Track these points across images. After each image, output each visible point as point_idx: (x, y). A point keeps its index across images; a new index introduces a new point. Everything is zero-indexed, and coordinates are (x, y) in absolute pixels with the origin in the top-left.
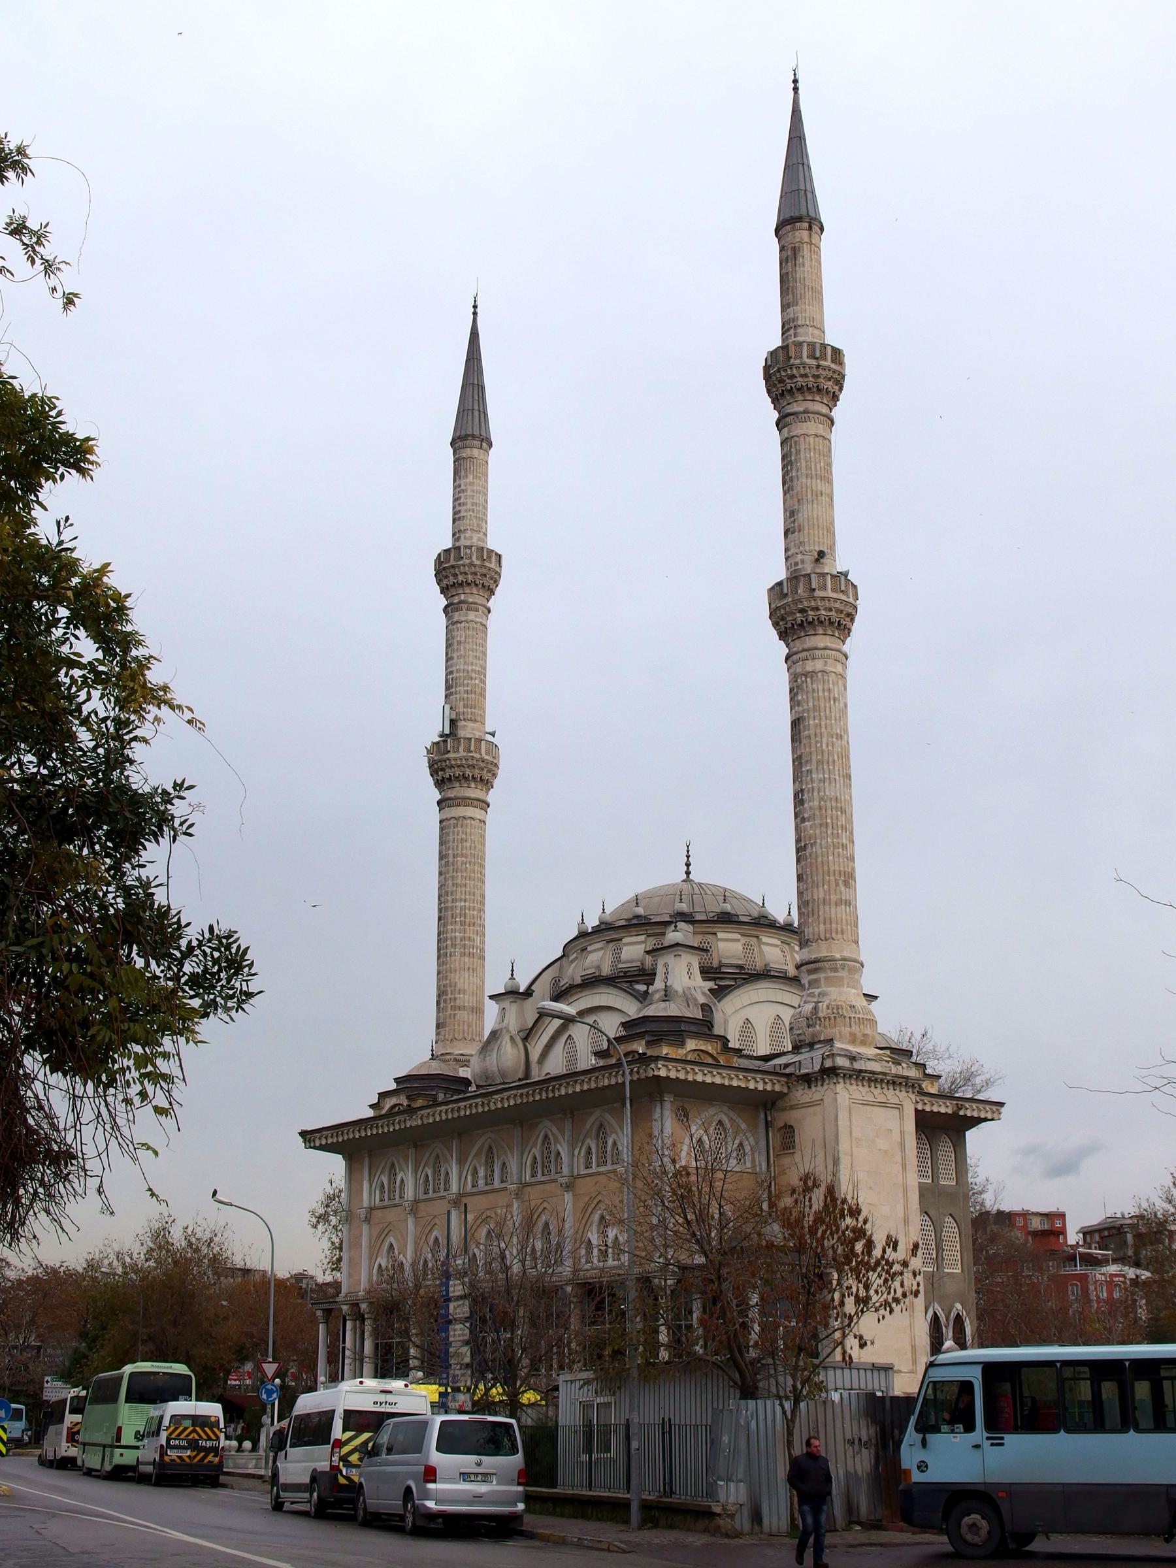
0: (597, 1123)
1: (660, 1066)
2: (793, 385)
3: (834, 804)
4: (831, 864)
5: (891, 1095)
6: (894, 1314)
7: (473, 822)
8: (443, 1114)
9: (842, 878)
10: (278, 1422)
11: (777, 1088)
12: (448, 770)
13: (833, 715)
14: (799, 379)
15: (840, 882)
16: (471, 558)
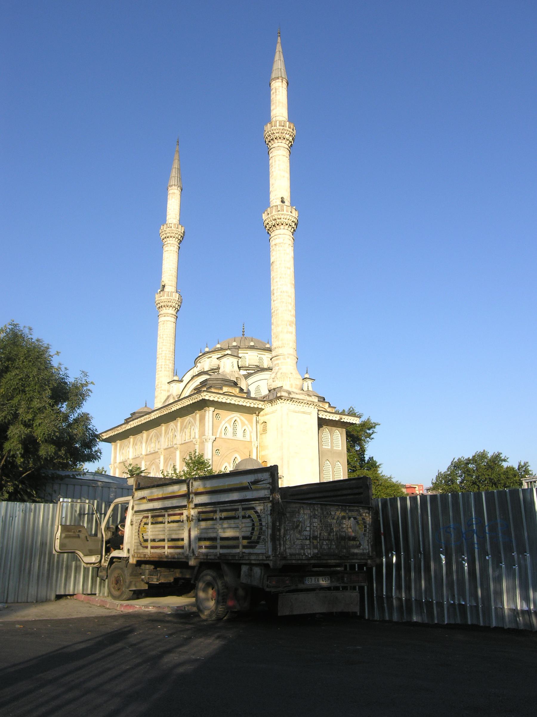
0: (188, 422)
2: (273, 137)
5: (306, 408)
6: (52, 360)
8: (137, 423)
10: (106, 554)
12: (161, 303)
14: (276, 134)
16: (171, 228)
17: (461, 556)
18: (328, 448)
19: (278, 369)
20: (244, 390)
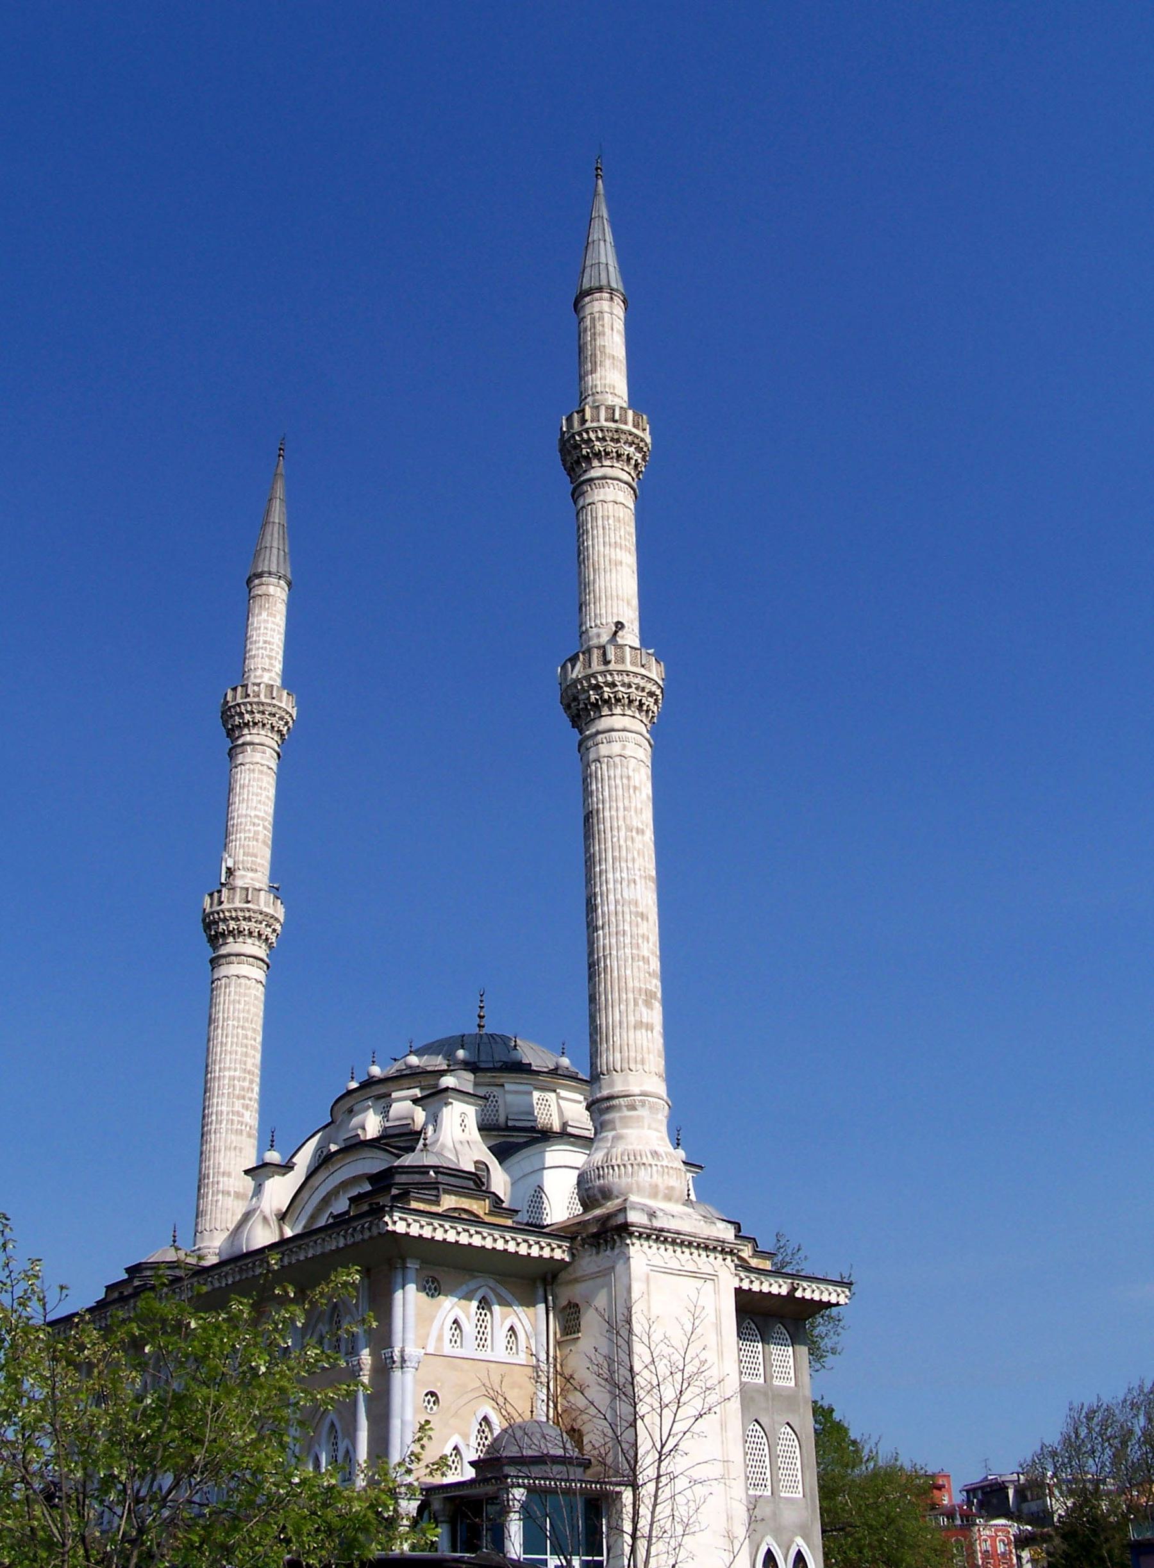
1: (396, 1218)
3: (633, 909)
4: (630, 981)
7: (247, 982)
9: (643, 997)
11: (558, 1254)
13: (633, 805)
15: (640, 1002)
16: (259, 696)
17: (566, 1566)
18: (756, 1381)
19: (613, 1138)
20: (503, 1202)
